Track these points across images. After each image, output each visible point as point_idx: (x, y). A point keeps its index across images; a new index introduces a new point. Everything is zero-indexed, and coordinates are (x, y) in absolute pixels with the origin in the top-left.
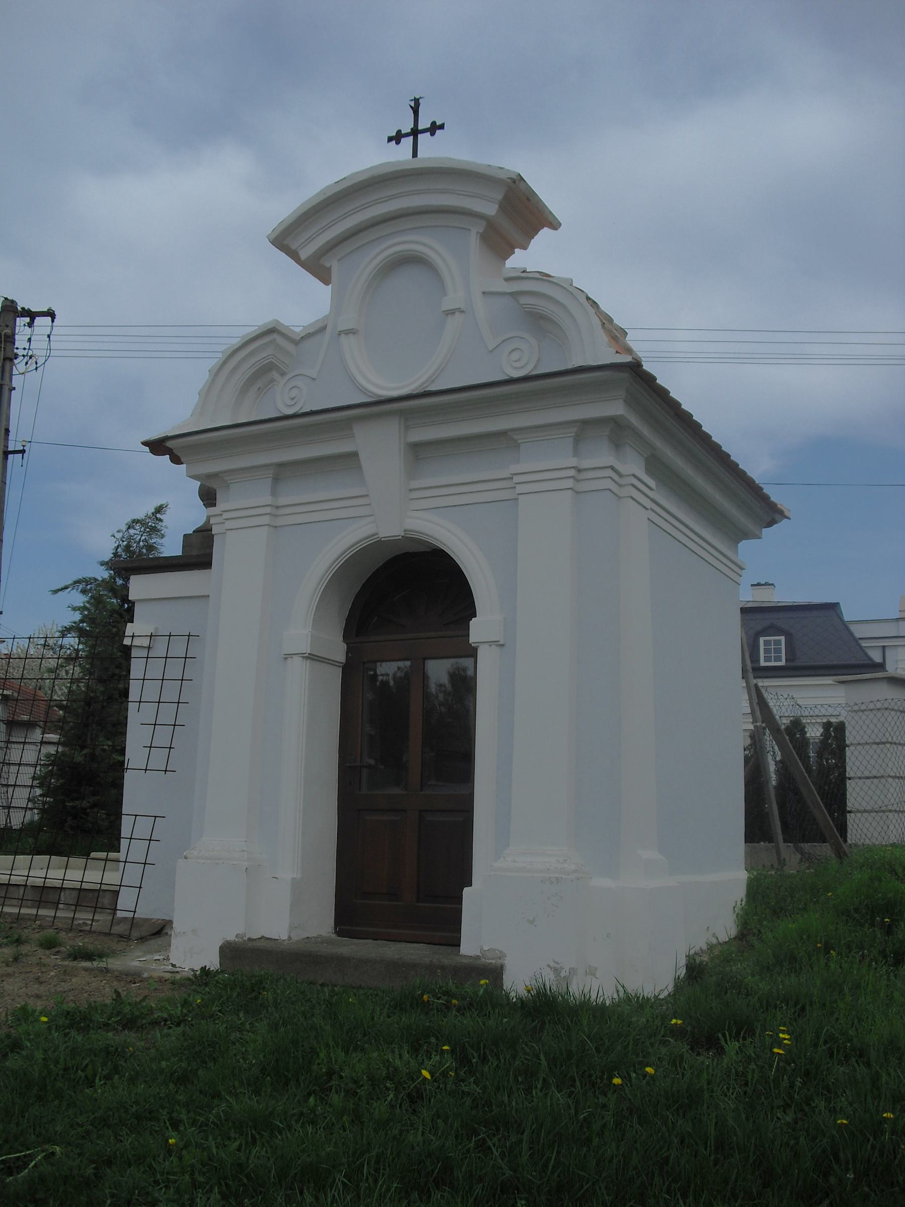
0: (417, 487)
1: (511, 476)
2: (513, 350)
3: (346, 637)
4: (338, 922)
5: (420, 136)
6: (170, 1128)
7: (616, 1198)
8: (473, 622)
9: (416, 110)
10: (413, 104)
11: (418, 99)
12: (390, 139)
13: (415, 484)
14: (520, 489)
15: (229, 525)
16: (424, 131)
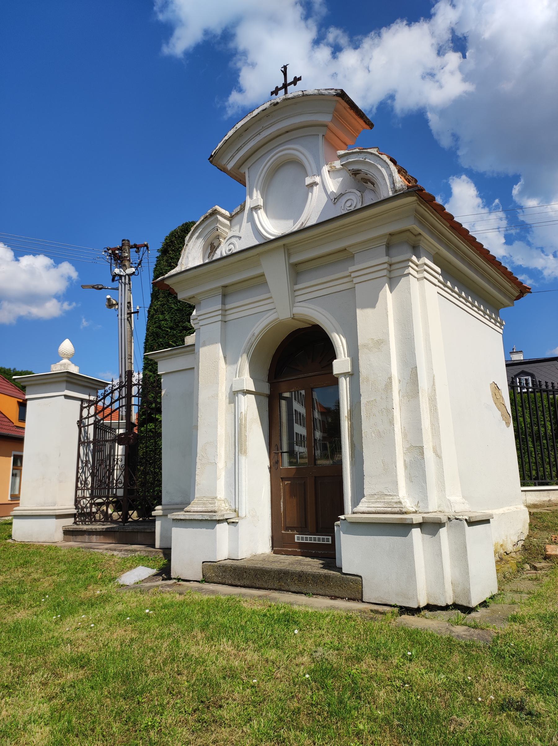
0: (396, 268)
1: (350, 274)
2: (348, 200)
3: (269, 381)
4: (273, 547)
5: (288, 87)
6: (292, 730)
7: (76, 551)
8: (335, 362)
9: (285, 73)
10: (283, 69)
11: (286, 66)
12: (300, 79)
13: (297, 287)
14: (356, 280)
15: (201, 323)
16: (290, 84)
